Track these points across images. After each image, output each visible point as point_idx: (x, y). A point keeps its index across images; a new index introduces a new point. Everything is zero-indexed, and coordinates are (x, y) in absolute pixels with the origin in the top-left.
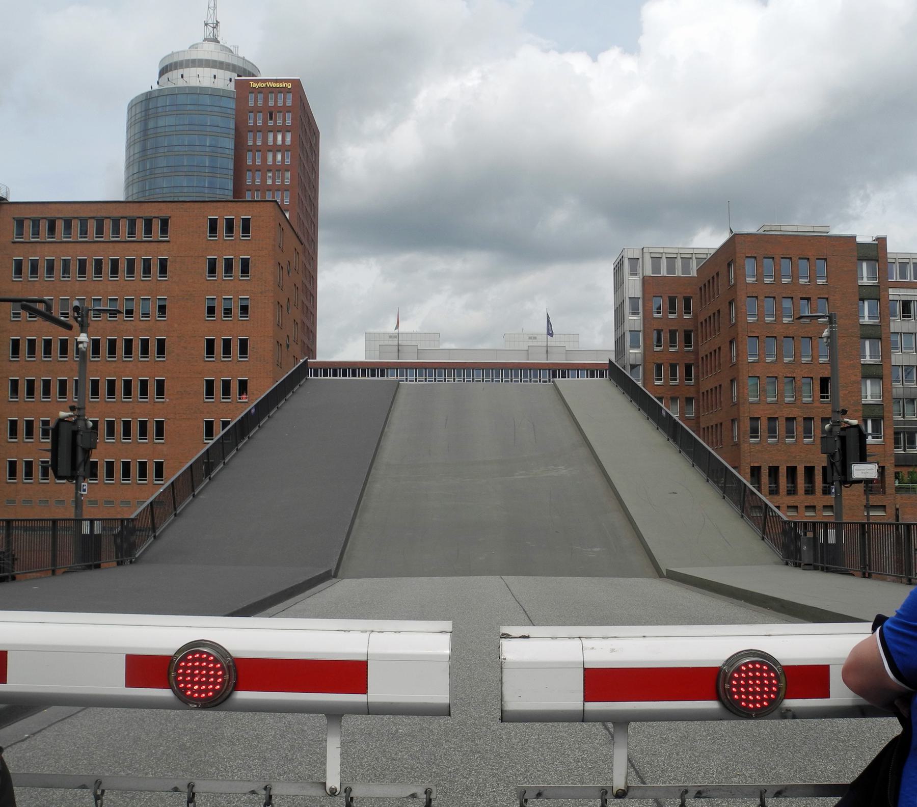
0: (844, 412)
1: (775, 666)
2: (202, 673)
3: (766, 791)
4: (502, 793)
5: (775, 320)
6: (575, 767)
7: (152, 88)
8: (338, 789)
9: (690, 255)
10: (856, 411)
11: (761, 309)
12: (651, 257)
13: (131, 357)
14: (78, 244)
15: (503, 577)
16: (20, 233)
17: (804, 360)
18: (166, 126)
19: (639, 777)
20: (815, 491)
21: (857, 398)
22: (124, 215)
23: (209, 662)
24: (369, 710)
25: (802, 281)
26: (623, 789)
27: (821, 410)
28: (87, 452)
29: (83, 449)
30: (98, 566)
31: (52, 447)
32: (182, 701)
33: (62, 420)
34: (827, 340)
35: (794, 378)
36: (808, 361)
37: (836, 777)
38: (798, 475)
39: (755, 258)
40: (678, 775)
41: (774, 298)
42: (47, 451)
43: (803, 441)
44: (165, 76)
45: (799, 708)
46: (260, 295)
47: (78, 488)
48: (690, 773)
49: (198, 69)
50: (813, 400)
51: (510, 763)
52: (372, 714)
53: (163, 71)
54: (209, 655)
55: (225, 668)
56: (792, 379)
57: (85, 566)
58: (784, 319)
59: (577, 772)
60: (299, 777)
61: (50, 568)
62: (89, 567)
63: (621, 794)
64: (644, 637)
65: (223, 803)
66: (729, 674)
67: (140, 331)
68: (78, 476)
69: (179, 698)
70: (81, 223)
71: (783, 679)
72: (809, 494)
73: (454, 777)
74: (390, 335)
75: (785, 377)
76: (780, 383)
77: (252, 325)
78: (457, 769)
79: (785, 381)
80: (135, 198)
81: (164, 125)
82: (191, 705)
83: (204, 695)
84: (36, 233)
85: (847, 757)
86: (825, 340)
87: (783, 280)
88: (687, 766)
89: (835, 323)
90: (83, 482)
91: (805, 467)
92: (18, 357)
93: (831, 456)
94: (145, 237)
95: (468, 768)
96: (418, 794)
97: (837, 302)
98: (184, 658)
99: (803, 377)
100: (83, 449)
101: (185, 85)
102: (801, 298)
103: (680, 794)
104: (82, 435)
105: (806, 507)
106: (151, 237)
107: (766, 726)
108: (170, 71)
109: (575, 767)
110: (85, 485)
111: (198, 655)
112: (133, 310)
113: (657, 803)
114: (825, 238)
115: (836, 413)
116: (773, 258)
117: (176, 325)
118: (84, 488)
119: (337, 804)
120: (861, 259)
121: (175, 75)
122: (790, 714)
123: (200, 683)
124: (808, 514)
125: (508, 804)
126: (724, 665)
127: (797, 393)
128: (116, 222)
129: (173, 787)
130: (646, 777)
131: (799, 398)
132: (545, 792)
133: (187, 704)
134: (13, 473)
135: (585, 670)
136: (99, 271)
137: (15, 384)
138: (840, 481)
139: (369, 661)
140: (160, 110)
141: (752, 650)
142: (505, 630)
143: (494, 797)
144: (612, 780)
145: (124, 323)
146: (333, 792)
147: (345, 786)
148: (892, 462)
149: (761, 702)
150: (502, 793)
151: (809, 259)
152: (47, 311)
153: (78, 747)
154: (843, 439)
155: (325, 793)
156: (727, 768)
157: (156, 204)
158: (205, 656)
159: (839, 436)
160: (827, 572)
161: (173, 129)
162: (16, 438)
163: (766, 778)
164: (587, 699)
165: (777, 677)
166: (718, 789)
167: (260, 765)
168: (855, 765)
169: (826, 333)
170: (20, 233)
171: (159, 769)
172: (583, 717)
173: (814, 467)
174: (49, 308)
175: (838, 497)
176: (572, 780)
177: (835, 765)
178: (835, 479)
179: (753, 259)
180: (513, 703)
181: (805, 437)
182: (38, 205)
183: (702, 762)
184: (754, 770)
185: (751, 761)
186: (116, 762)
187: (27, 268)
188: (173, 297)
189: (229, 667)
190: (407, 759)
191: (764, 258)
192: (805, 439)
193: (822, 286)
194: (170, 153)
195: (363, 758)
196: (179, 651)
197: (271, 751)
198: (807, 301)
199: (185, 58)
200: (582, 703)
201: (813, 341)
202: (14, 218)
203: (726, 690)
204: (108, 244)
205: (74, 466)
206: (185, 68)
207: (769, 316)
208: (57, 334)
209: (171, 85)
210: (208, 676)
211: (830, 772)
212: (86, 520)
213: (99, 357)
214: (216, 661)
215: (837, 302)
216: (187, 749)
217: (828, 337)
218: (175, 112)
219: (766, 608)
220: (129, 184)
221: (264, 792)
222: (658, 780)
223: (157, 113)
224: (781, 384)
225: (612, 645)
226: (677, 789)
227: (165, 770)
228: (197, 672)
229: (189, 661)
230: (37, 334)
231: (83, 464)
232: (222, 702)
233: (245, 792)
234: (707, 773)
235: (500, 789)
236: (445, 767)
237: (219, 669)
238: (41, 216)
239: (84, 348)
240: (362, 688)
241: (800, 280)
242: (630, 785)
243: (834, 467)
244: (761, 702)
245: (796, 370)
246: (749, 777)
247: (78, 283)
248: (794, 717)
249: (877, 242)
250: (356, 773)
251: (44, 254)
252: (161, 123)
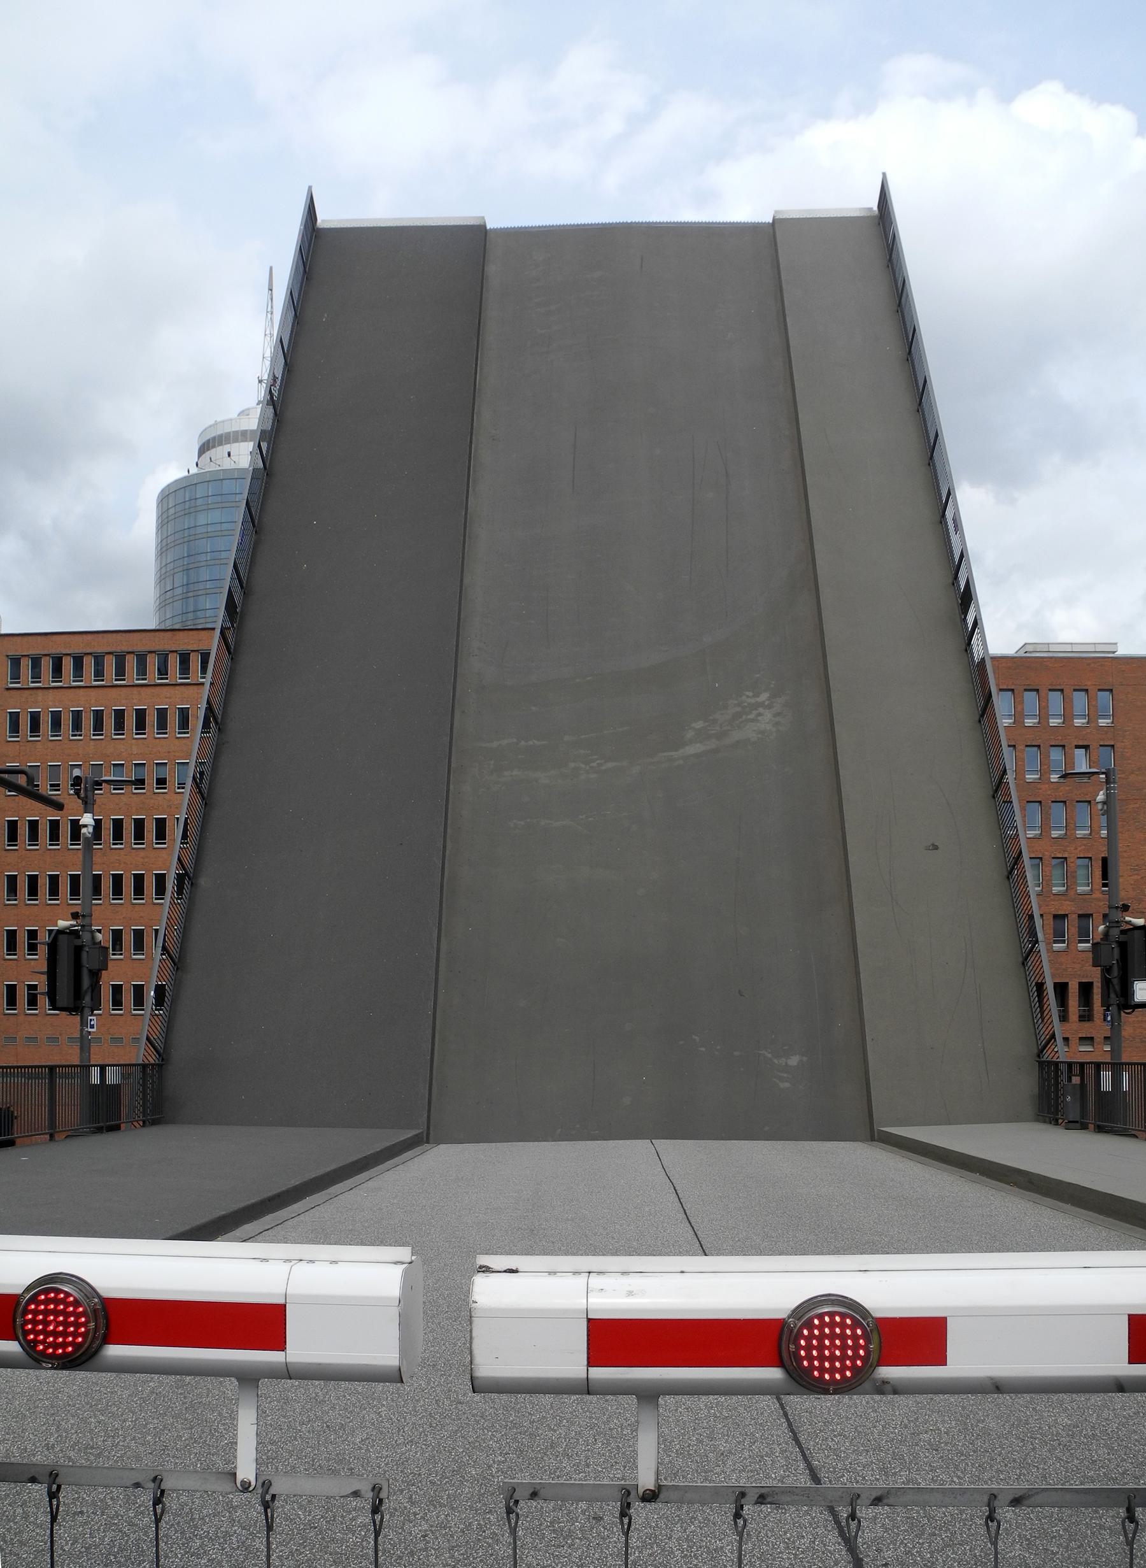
0: (1125, 908)
1: (863, 1319)
2: (58, 1320)
3: (859, 1495)
4: (599, 1453)
5: (1040, 779)
6: (705, 1416)
7: (189, 471)
8: (253, 1483)
11: (1020, 763)
12: (1030, 858)
13: (165, 843)
14: (92, 689)
15: (653, 1141)
16: (16, 676)
17: (1080, 833)
18: (208, 524)
19: (792, 1431)
20: (1093, 1017)
22: (153, 649)
23: (67, 1305)
24: (289, 1373)
25: (1078, 722)
26: (653, 1489)
27: (1102, 903)
28: (95, 975)
29: (90, 971)
30: (117, 1128)
31: (48, 970)
32: (33, 1359)
33: (60, 932)
34: (1103, 807)
35: (1066, 858)
36: (1085, 834)
37: (1068, 1435)
38: (1070, 994)
39: (1012, 690)
40: (846, 1430)
41: (1039, 746)
42: (42, 973)
43: (1077, 947)
44: (208, 454)
45: (900, 1380)
47: (84, 1023)
48: (864, 1426)
49: (242, 444)
50: (1091, 890)
51: (617, 1409)
52: (296, 1379)
53: (204, 449)
54: (68, 1295)
55: (90, 1313)
56: (1063, 860)
57: (94, 1128)
58: (1051, 776)
59: (707, 1423)
60: (328, 1426)
61: (47, 1131)
62: (99, 1130)
63: (651, 1497)
64: (682, 1272)
65: (218, 1463)
66: (796, 1330)
67: (177, 808)
68: (83, 1007)
69: (28, 1353)
70: (201, 656)
71: (875, 1338)
72: (1085, 1021)
73: (537, 1428)
75: (1053, 858)
76: (1047, 867)
78: (544, 1417)
79: (1053, 864)
80: (168, 625)
81: (206, 523)
82: (44, 1365)
83: (60, 1351)
84: (36, 676)
85: (1089, 1405)
86: (1100, 806)
87: (1051, 721)
88: (861, 1416)
89: (1114, 783)
90: (90, 1016)
91: (1079, 982)
92: (16, 845)
93: (1107, 970)
94: (180, 678)
95: (559, 1416)
96: (363, 1492)
97: (1126, 750)
98: (34, 1299)
99: (1078, 858)
100: (90, 971)
101: (233, 466)
102: (1076, 745)
103: (734, 1498)
104: (87, 952)
105: (1081, 1039)
106: (188, 678)
107: (857, 1403)
108: (219, 445)
109: (705, 1416)
110: (93, 1020)
111: (52, 1295)
112: (166, 778)
113: (809, 1470)
114: (1110, 659)
115: (1114, 910)
116: (1037, 690)
118: (92, 1023)
119: (372, 1466)
121: (219, 452)
122: (888, 1388)
123: (55, 1334)
124: (1082, 1049)
125: (603, 1468)
126: (789, 1317)
127: (1070, 880)
128: (142, 659)
129: (29, 1477)
130: (802, 1431)
131: (1072, 887)
132: (542, 1491)
133: (38, 1363)
134: (12, 1001)
135: (590, 1321)
136: (120, 726)
137: (12, 880)
138: (1118, 1005)
139: (287, 1305)
140: (199, 502)
141: (830, 1295)
142: (483, 1260)
143: (587, 1458)
144: (636, 1478)
145: (153, 796)
146: (246, 1487)
147: (264, 1478)
149: (842, 1371)
150: (599, 1453)
151: (1087, 690)
152: (28, 785)
153: (41, 1383)
154: (1123, 946)
155: (235, 1488)
156: (917, 1419)
157: (194, 632)
158: (62, 1296)
159: (1117, 942)
160: (1099, 1132)
161: (218, 527)
162: (15, 955)
163: (969, 1435)
164: (592, 1362)
165: (865, 1335)
166: (789, 1492)
167: (279, 1409)
168: (1099, 1417)
169: (1101, 797)
170: (16, 676)
171: (143, 1415)
172: (587, 1388)
173: (1092, 983)
174: (31, 780)
175: (1116, 1026)
176: (697, 1434)
177: (1069, 1417)
178: (1112, 1003)
179: (1010, 693)
180: (488, 1367)
181: (1080, 942)
182: (39, 637)
183: (882, 1410)
184: (953, 1423)
185: (952, 1409)
186: (87, 1403)
187: (25, 723)
189: (95, 1311)
190: (477, 1402)
191: (1026, 690)
192: (1079, 945)
193: (1105, 729)
194: (213, 562)
195: (417, 1401)
196: (29, 1289)
197: (297, 1389)
198: (1084, 750)
199: (233, 430)
200: (586, 1368)
201: (1092, 806)
202: (8, 656)
203: (791, 1353)
204: (131, 688)
205: (78, 994)
206: (233, 443)
207: (1032, 772)
208: (44, 816)
209: (213, 468)
210: (66, 1324)
211: (1061, 1427)
212: (95, 1066)
213: (122, 844)
214: (76, 1303)
215: (1126, 750)
216: (185, 1385)
217: (1104, 803)
218: (220, 505)
219: (1008, 1183)
220: (163, 603)
221: (152, 1485)
222: (817, 1436)
223: (196, 506)
224: (1048, 868)
225: (630, 1285)
226: (731, 1490)
227: (150, 1416)
228: (52, 1318)
229: (42, 1302)
230: (41, 814)
231: (90, 990)
232: (87, 1360)
233: (128, 1485)
234: (887, 1426)
235: (597, 1446)
236: (527, 1415)
237: (83, 1314)
238: (43, 653)
239: (89, 833)
240: (278, 1342)
241: (1075, 721)
242: (665, 1483)
243: (1111, 986)
244: (842, 1371)
246: (945, 1433)
247: (92, 743)
248: (895, 1392)
250: (405, 1422)
251: (47, 704)
252: (202, 519)
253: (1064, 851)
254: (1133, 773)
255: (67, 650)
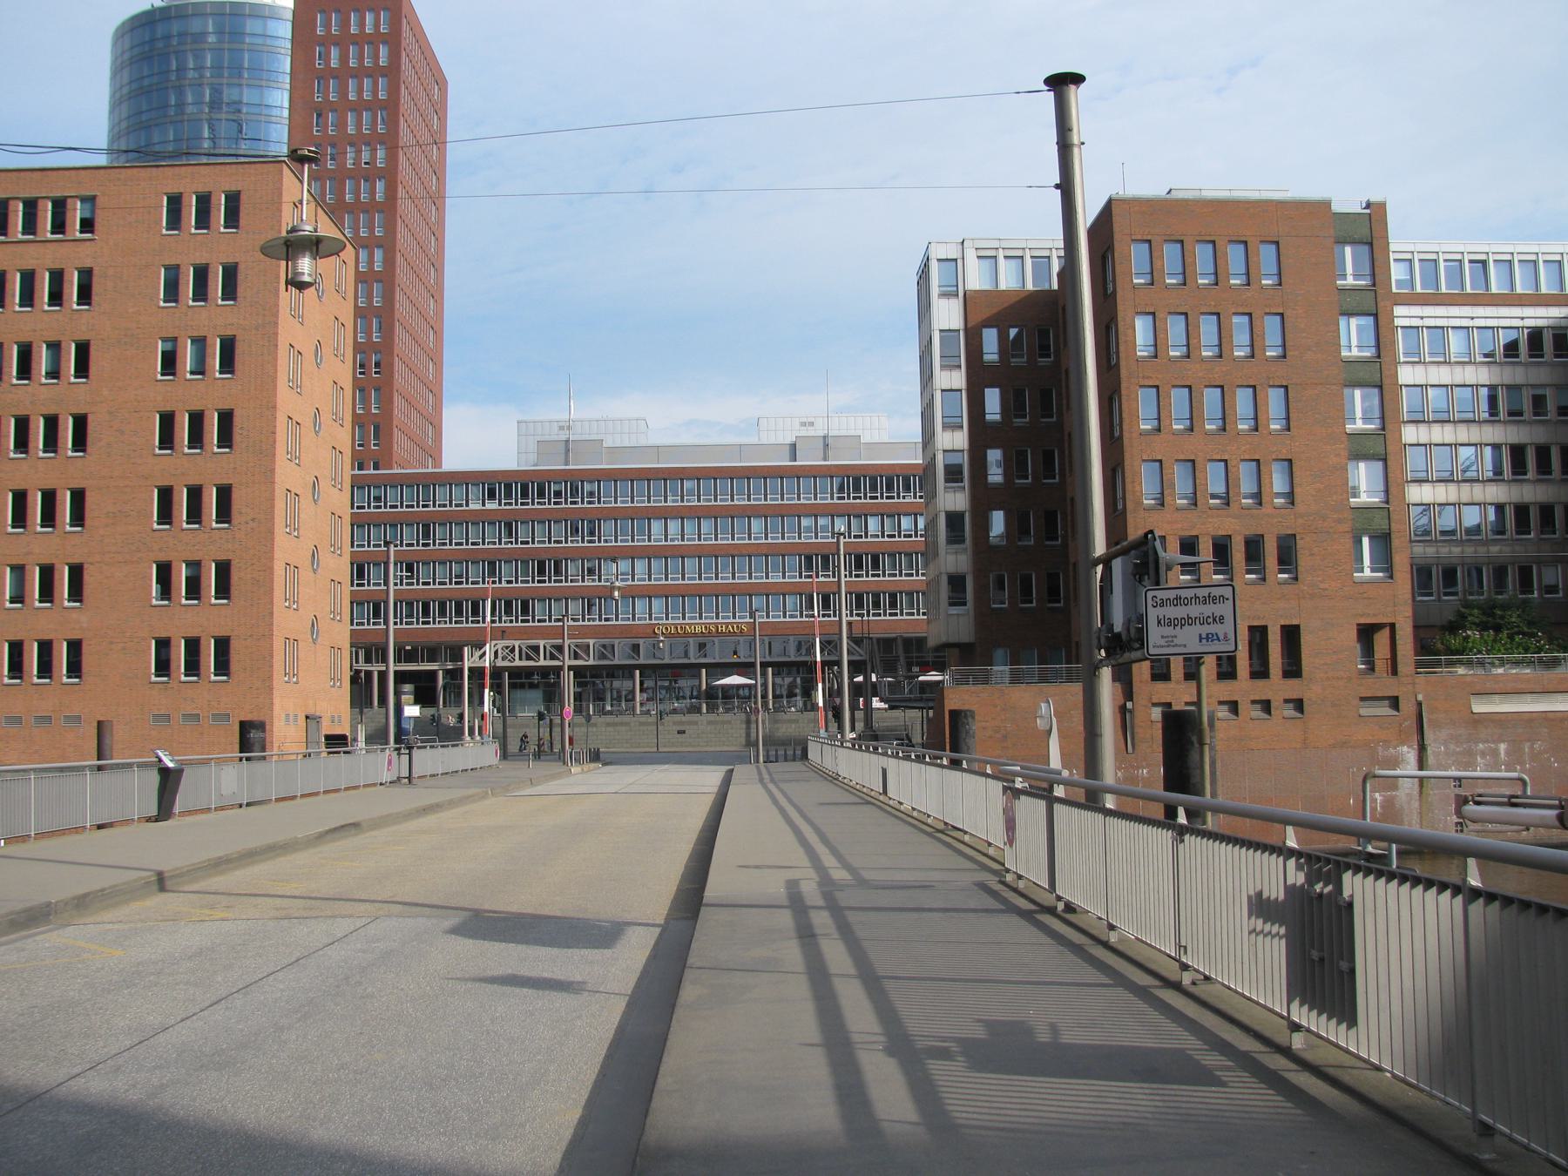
9: (1048, 251)
10: (1339, 521)
12: (978, 257)
21: (1341, 497)
46: (254, 332)
74: (561, 424)
77: (240, 387)
117: (105, 392)
120: (1342, 241)
148: (1407, 614)
188: (102, 340)
220: (108, 145)
245: (1228, 448)
249: (1368, 211)
253: (1222, 451)
254: (1309, 350)
255: (1432, 757)
